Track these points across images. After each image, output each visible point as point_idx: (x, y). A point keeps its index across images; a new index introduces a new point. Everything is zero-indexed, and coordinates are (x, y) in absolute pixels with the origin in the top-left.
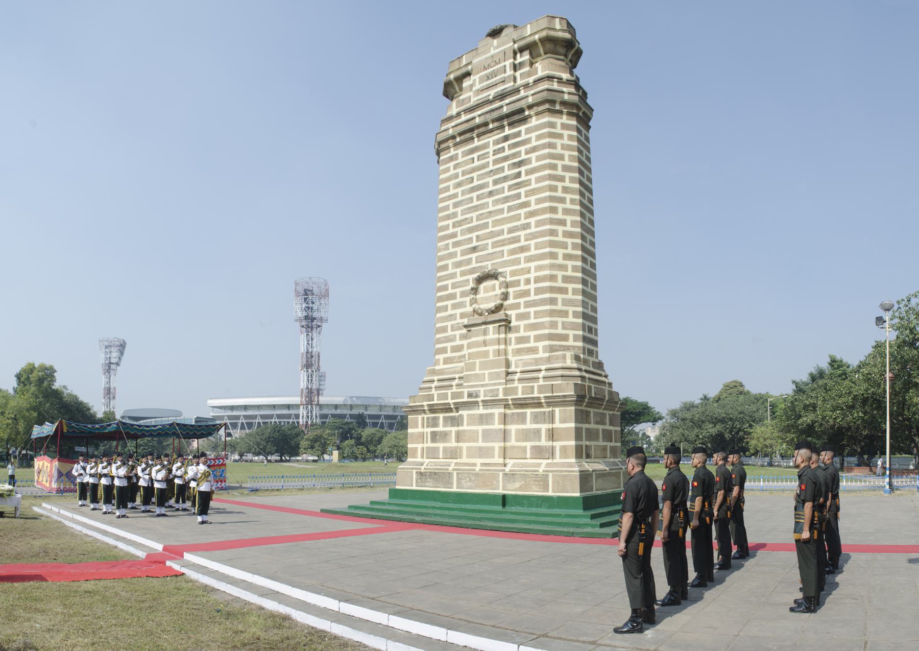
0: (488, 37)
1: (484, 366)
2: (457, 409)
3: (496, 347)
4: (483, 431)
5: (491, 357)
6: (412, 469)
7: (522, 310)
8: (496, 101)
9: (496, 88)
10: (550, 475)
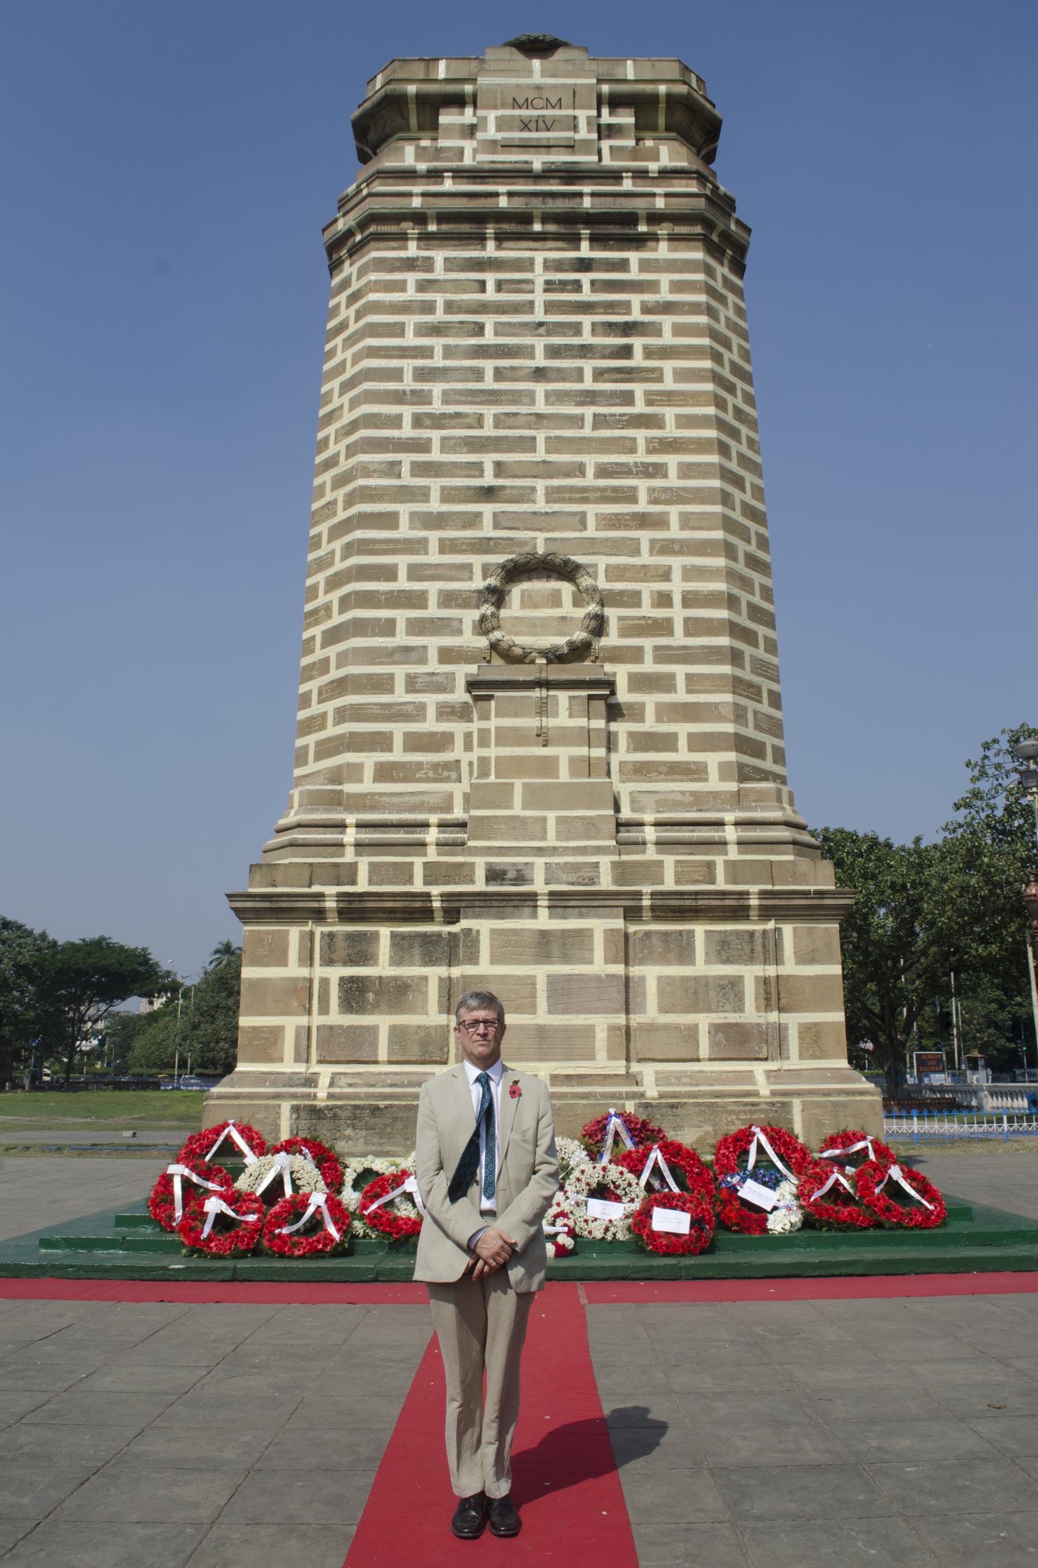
0: (514, 49)
1: (535, 797)
2: (452, 916)
3: (582, 751)
4: (552, 981)
5: (564, 775)
6: (277, 1096)
7: (648, 666)
8: (552, 181)
9: (548, 154)
10: (797, 1103)
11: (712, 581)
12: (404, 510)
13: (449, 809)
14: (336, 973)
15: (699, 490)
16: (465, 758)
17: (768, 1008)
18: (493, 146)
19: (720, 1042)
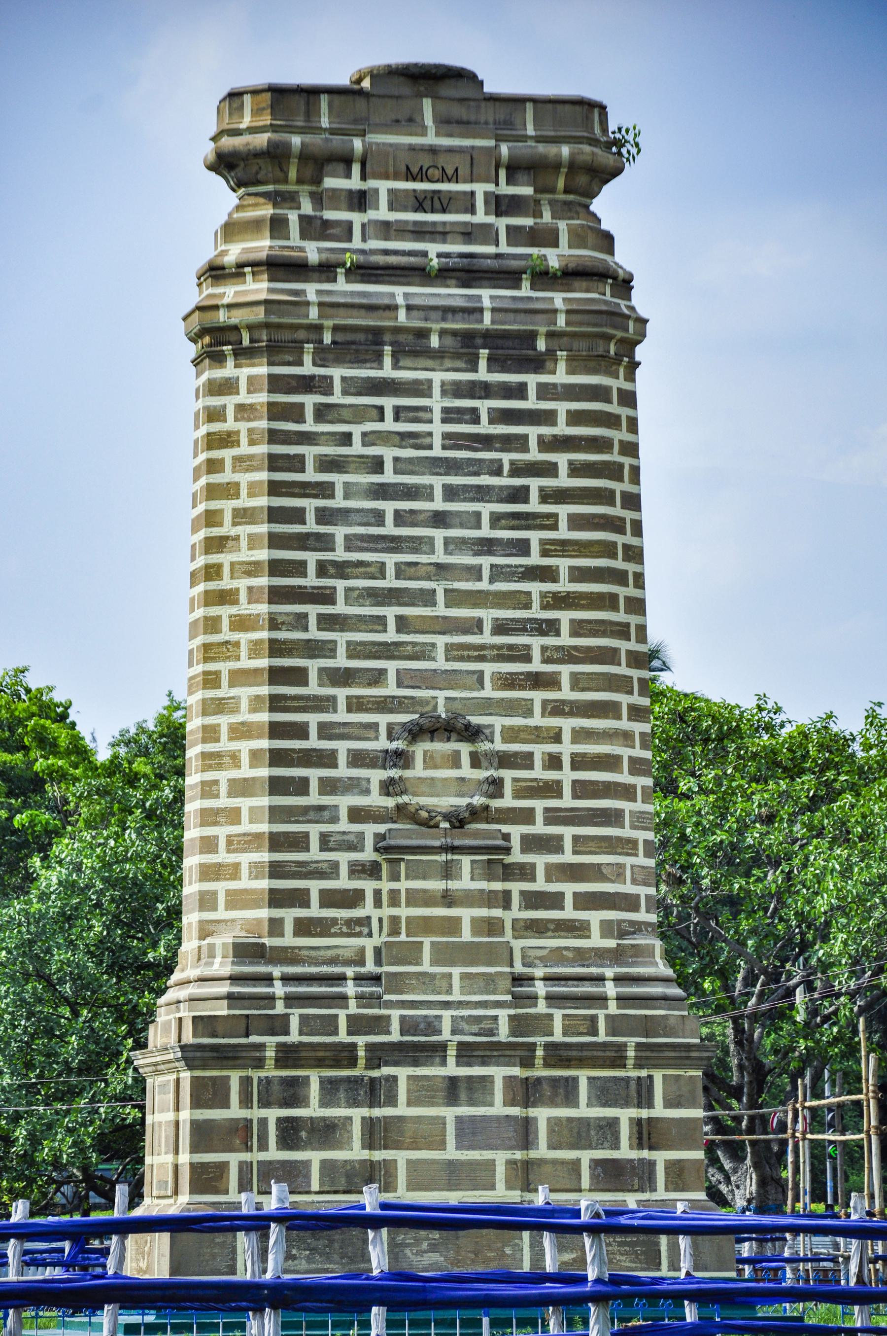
1: (443, 955)
2: (374, 1062)
7: (540, 828)
11: (598, 744)
12: (313, 666)
13: (362, 962)
14: (273, 1114)
15: (589, 649)
16: (375, 914)
17: (640, 1146)
18: (386, 229)
19: (599, 1175)
